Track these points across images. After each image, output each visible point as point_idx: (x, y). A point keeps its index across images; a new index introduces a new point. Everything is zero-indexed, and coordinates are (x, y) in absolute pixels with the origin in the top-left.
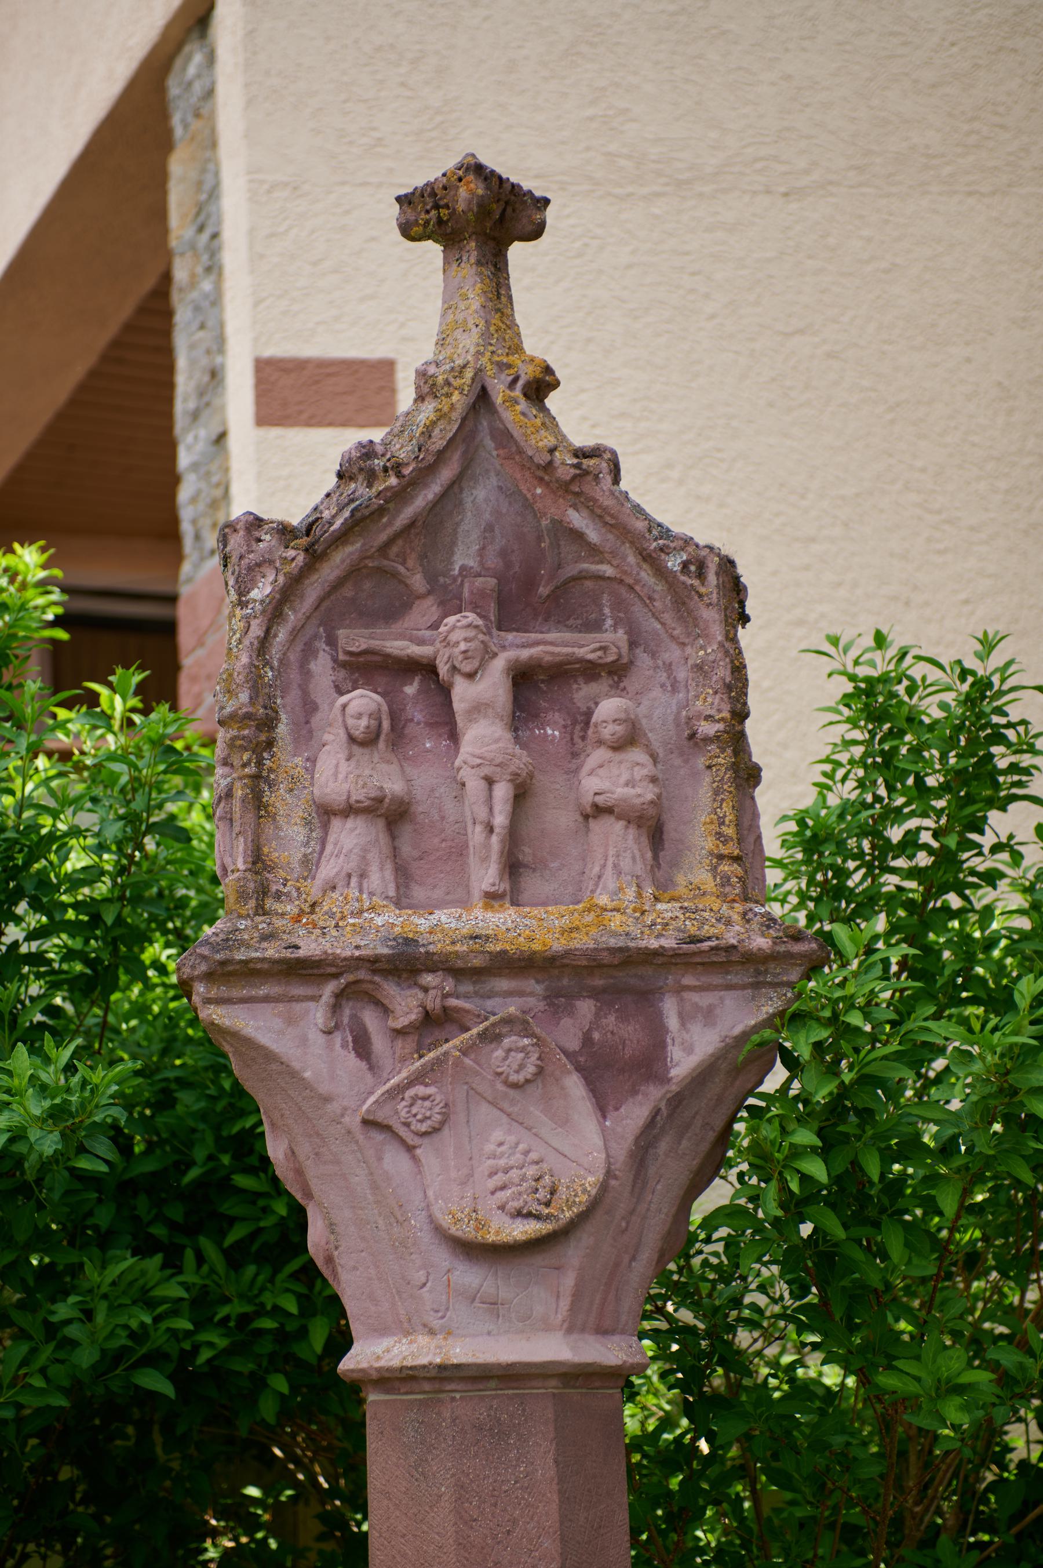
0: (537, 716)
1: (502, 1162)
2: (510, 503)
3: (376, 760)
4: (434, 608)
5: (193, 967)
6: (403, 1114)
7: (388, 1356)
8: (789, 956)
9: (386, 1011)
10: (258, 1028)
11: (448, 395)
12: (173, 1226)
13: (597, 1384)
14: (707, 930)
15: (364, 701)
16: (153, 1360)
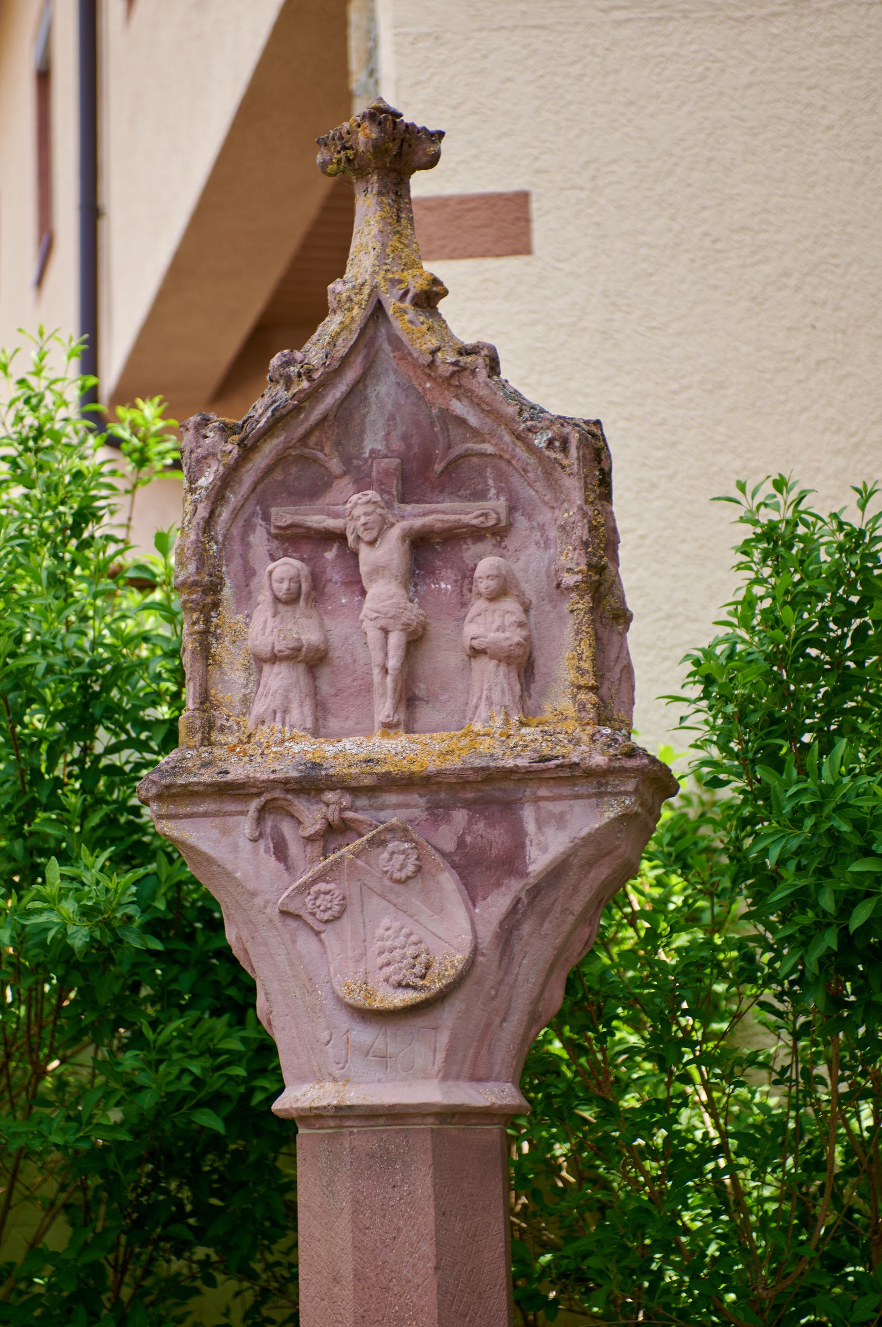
0: (433, 573)
1: (388, 944)
2: (407, 396)
3: (297, 616)
4: (350, 485)
5: (147, 790)
6: (309, 906)
7: (303, 1099)
8: (623, 770)
10: (199, 838)
11: (350, 310)
13: (473, 1121)
15: (286, 568)
16: (215, 1101)
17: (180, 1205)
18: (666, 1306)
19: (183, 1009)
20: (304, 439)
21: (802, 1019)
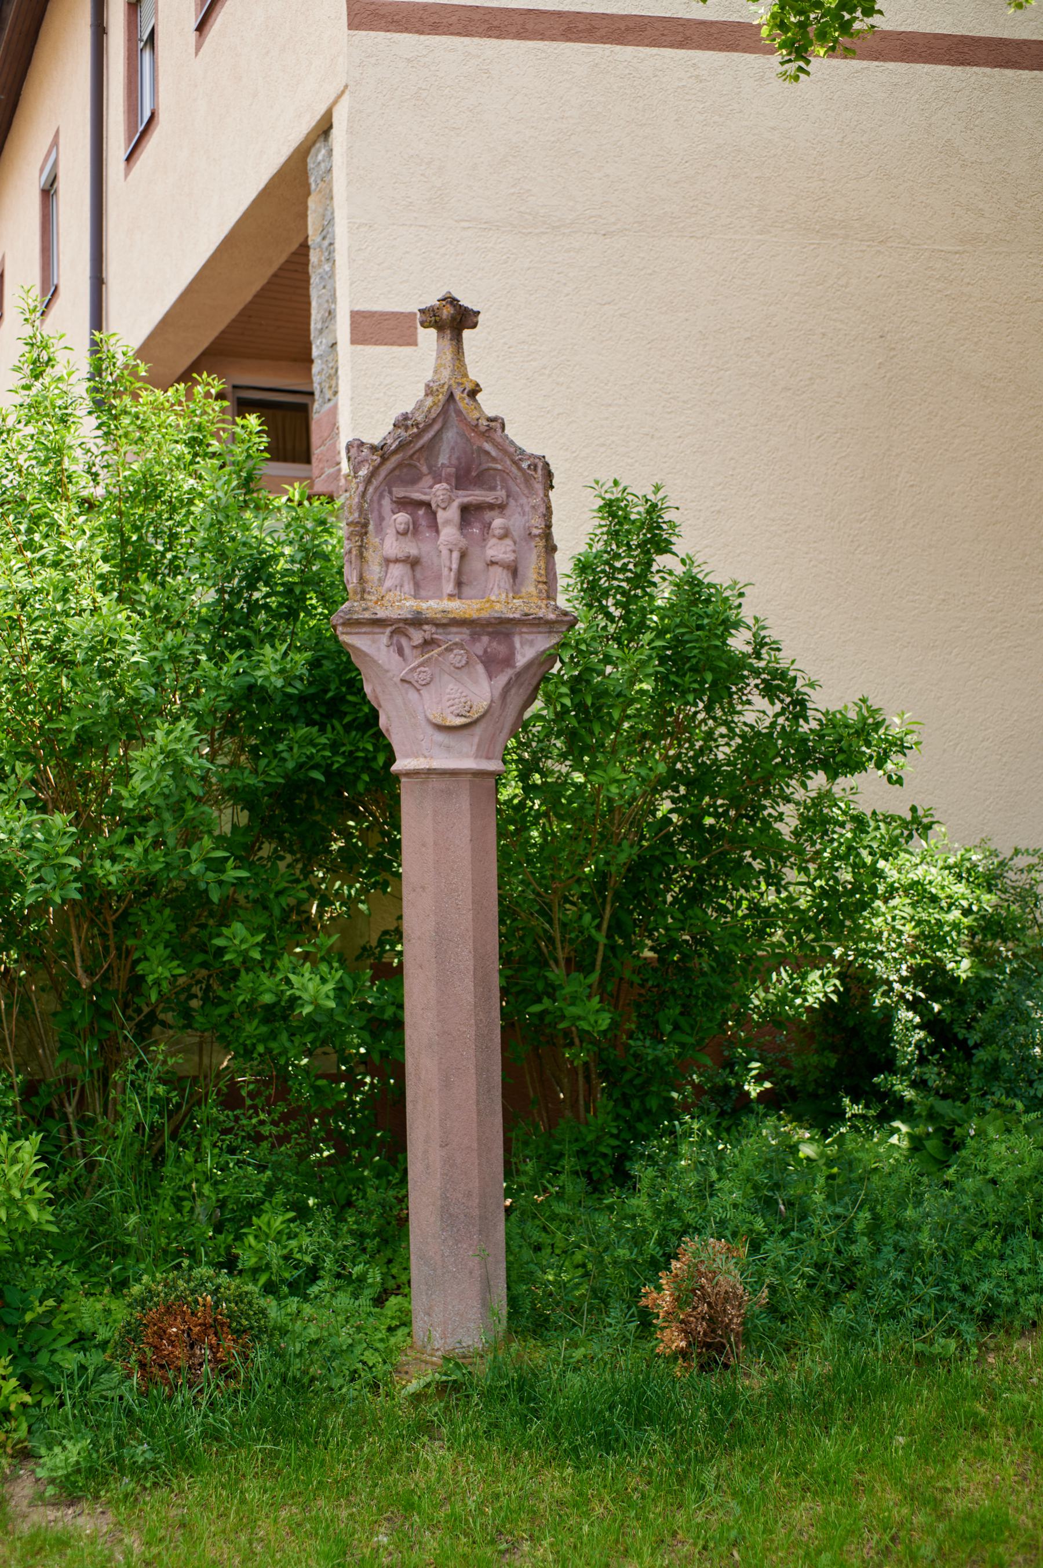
8: (562, 622)
9: (410, 639)
12: (322, 715)
16: (316, 767)
20: (411, 457)
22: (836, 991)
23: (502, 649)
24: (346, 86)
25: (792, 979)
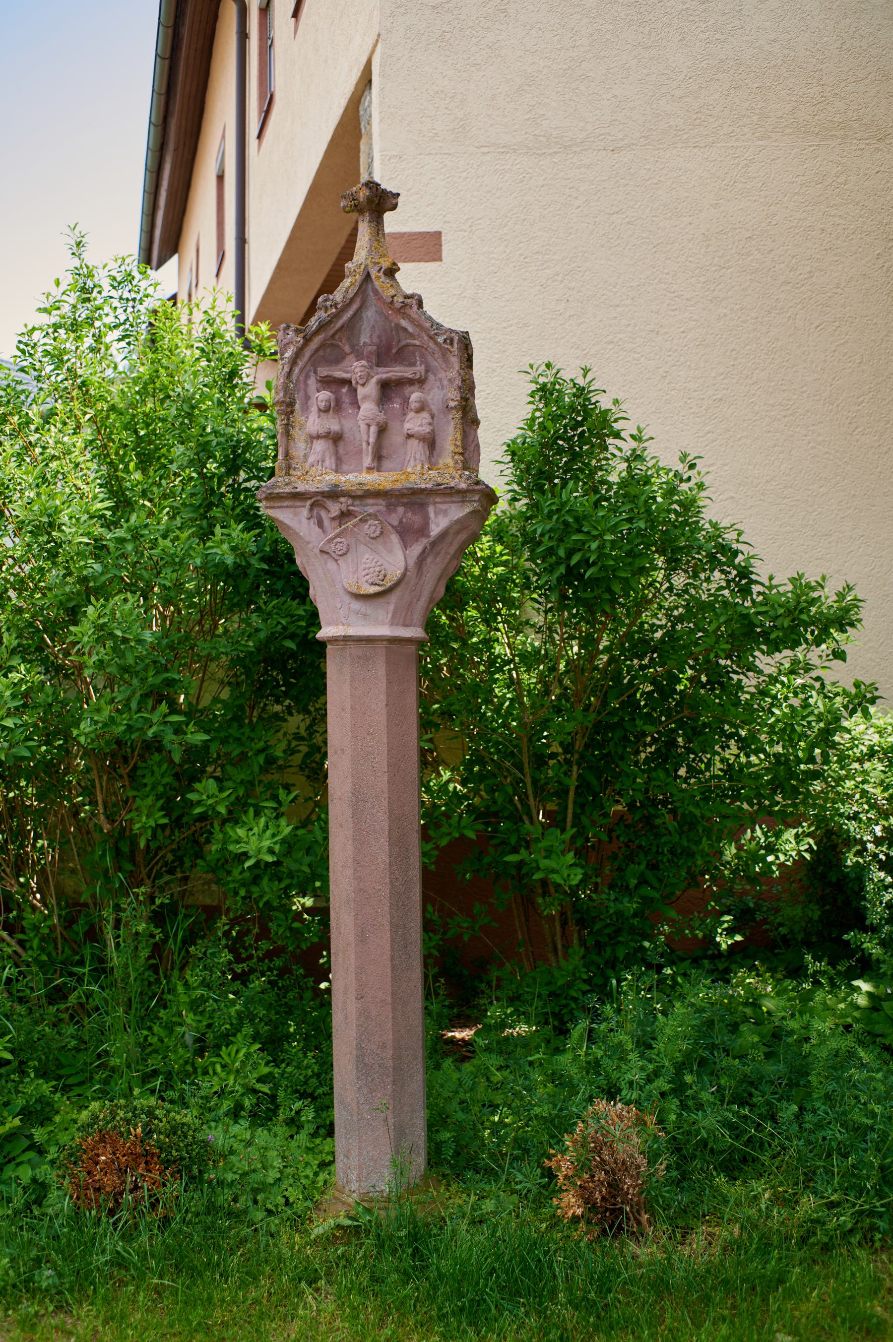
8: (474, 490)
14: (445, 481)
16: (292, 636)
17: (278, 682)
18: (486, 726)
19: (278, 596)
21: (549, 605)
22: (810, 850)
23: (416, 519)
24: (379, 35)
25: (767, 837)
